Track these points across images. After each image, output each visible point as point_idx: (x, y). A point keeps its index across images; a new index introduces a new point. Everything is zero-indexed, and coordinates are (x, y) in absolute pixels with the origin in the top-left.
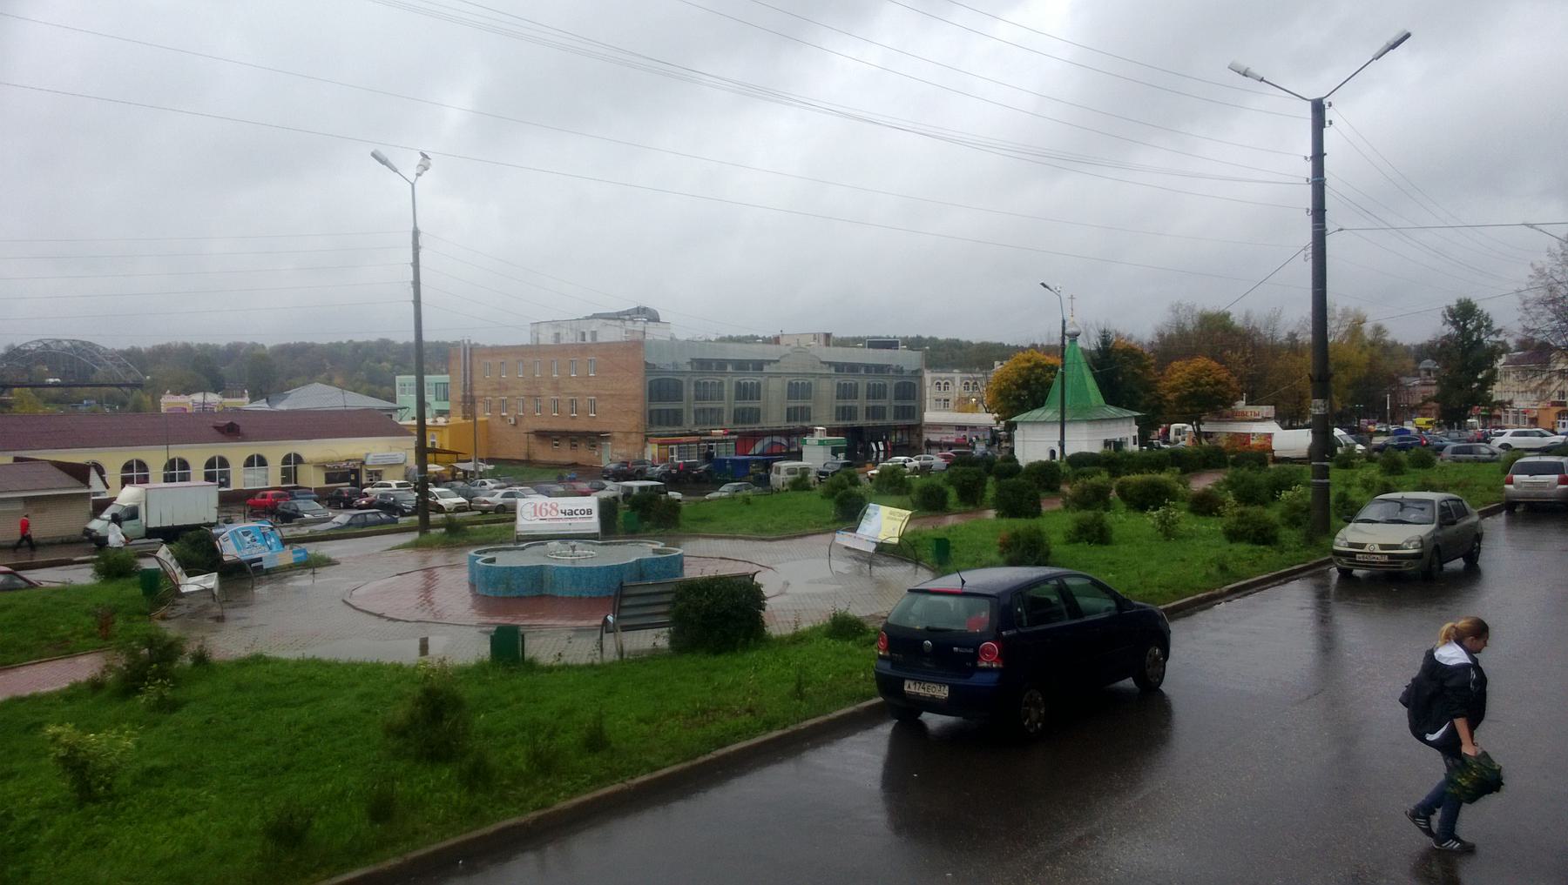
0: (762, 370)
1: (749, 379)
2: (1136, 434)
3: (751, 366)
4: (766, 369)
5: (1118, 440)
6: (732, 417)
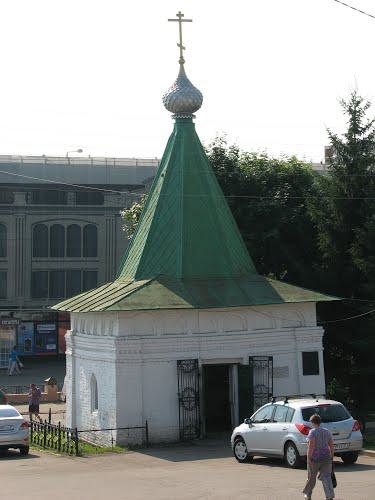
0: (101, 201)
1: (67, 218)
2: (318, 346)
3: (71, 195)
4: (110, 201)
5: (246, 362)
6: (28, 285)
